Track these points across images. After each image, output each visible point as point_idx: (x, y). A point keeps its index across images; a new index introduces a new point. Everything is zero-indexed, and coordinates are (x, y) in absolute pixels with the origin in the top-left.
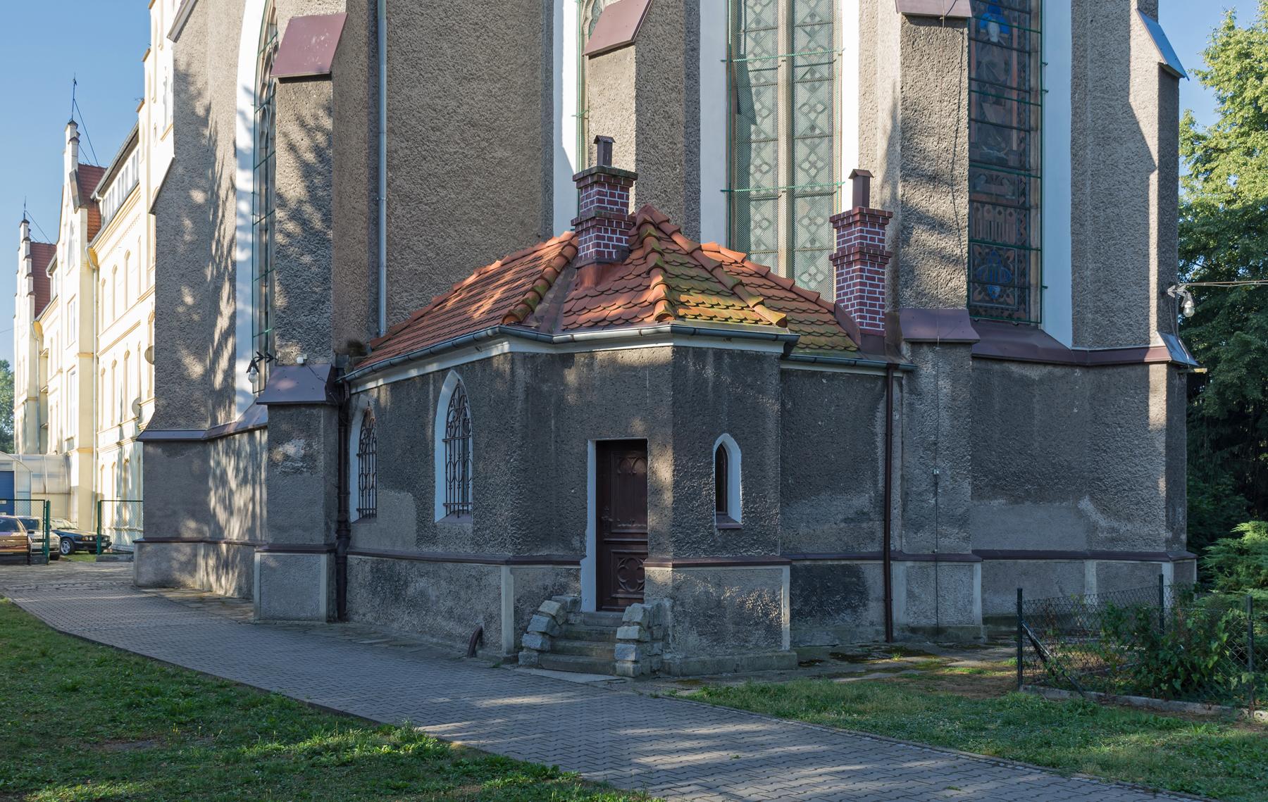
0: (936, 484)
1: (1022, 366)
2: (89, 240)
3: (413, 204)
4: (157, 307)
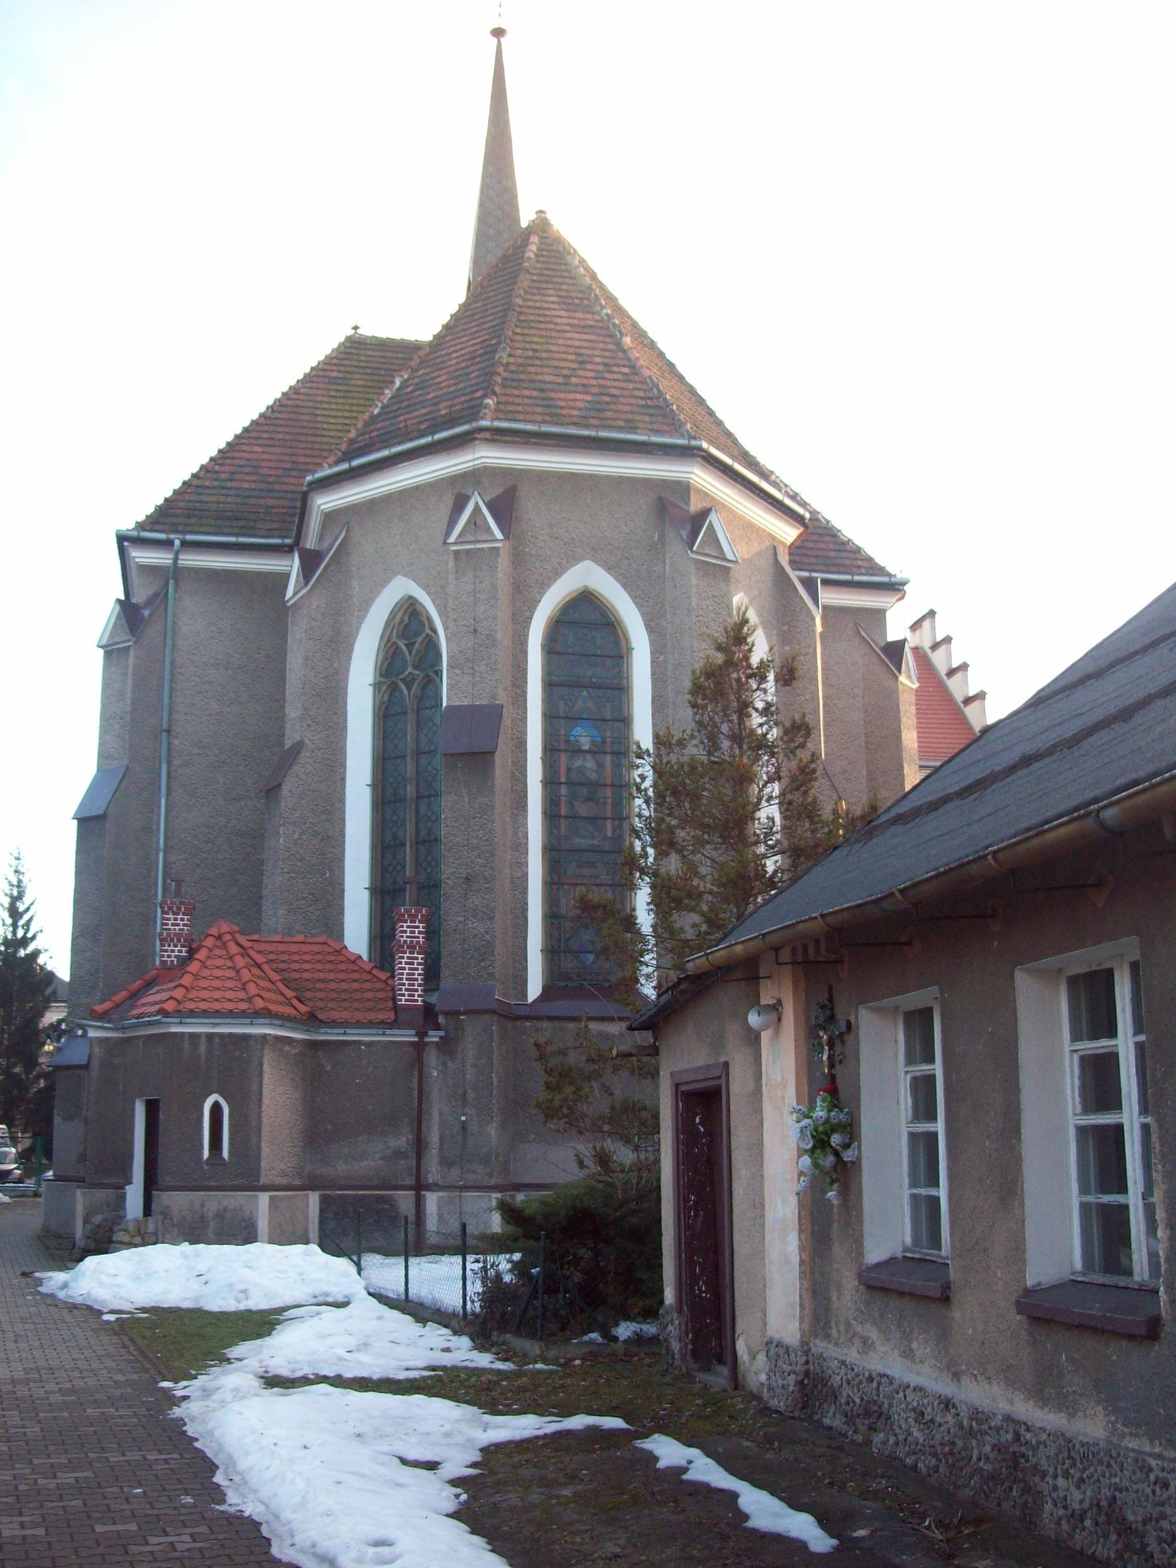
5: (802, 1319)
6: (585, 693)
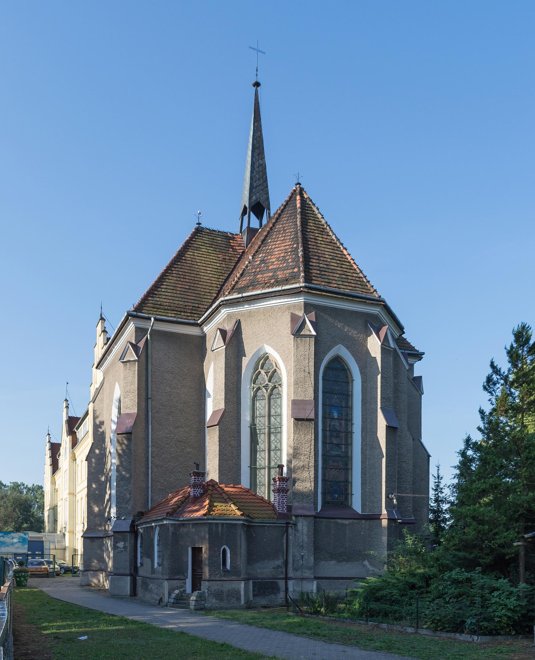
0: (302, 558)
1: (342, 520)
2: (72, 448)
3: (159, 468)
4: (88, 493)
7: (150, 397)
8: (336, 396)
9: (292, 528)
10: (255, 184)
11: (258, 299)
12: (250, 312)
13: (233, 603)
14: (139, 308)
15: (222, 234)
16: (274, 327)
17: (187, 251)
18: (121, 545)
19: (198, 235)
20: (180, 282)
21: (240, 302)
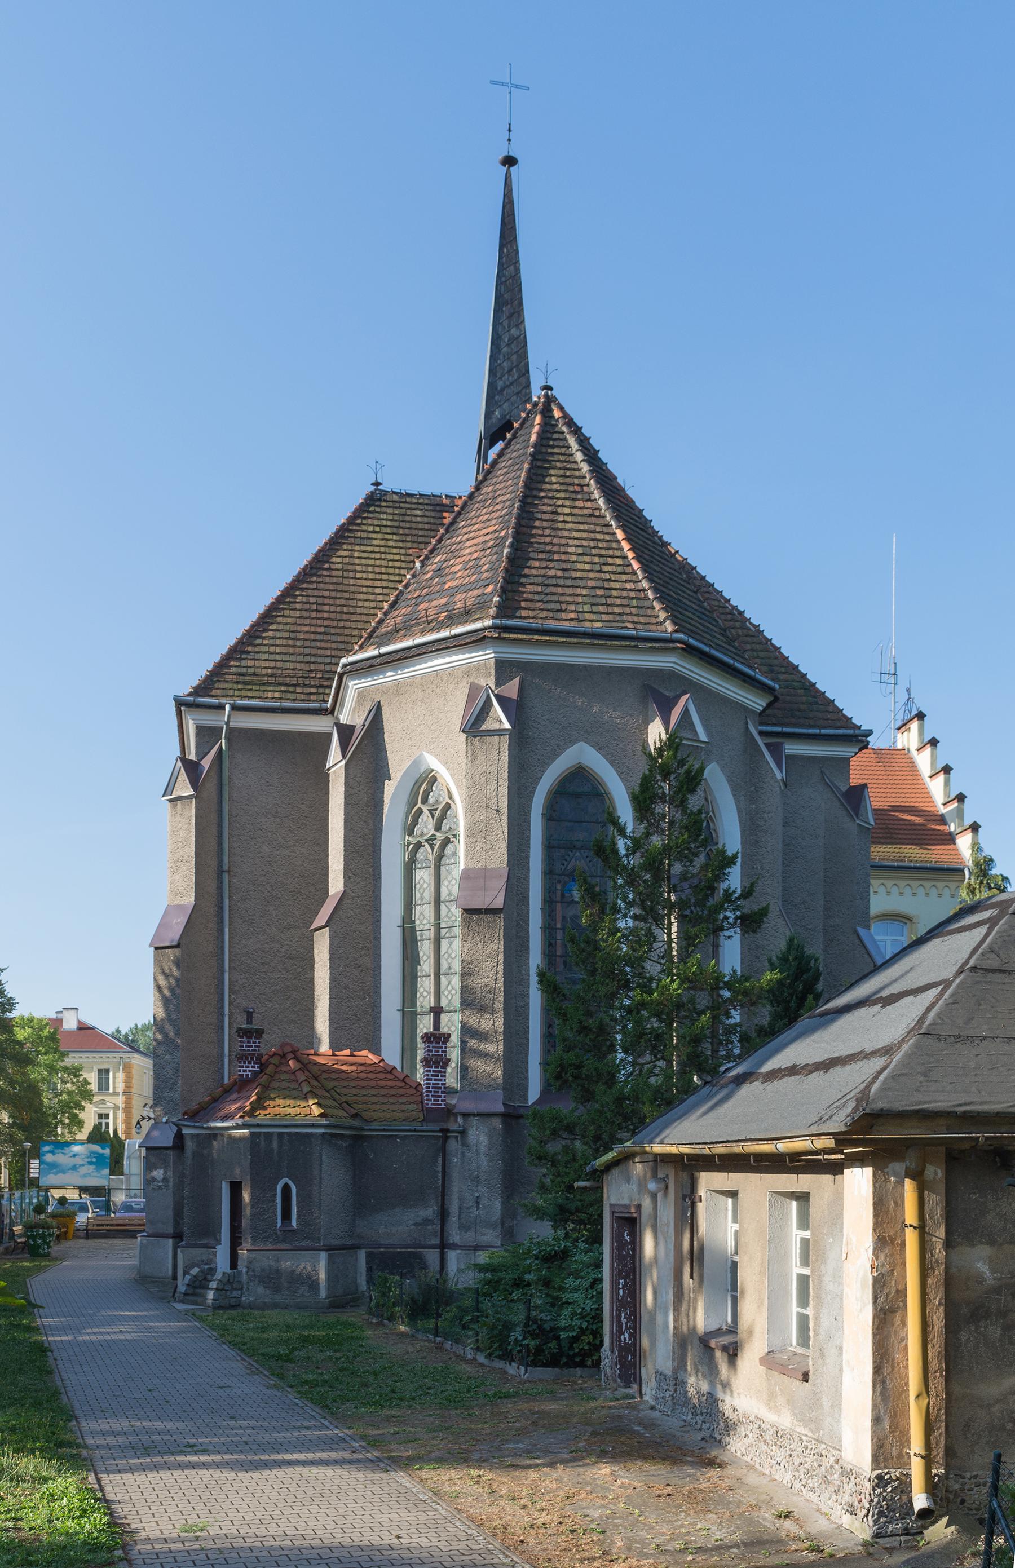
0: (477, 1202)
5: (673, 1360)
6: (578, 854)
7: (226, 868)
8: (578, 854)
9: (457, 1141)
10: (500, 384)
11: (407, 658)
12: (398, 684)
13: (303, 1295)
14: (204, 688)
15: (427, 501)
16: (441, 715)
17: (338, 550)
18: (158, 1174)
19: (372, 509)
20: (307, 621)
21: (374, 666)
